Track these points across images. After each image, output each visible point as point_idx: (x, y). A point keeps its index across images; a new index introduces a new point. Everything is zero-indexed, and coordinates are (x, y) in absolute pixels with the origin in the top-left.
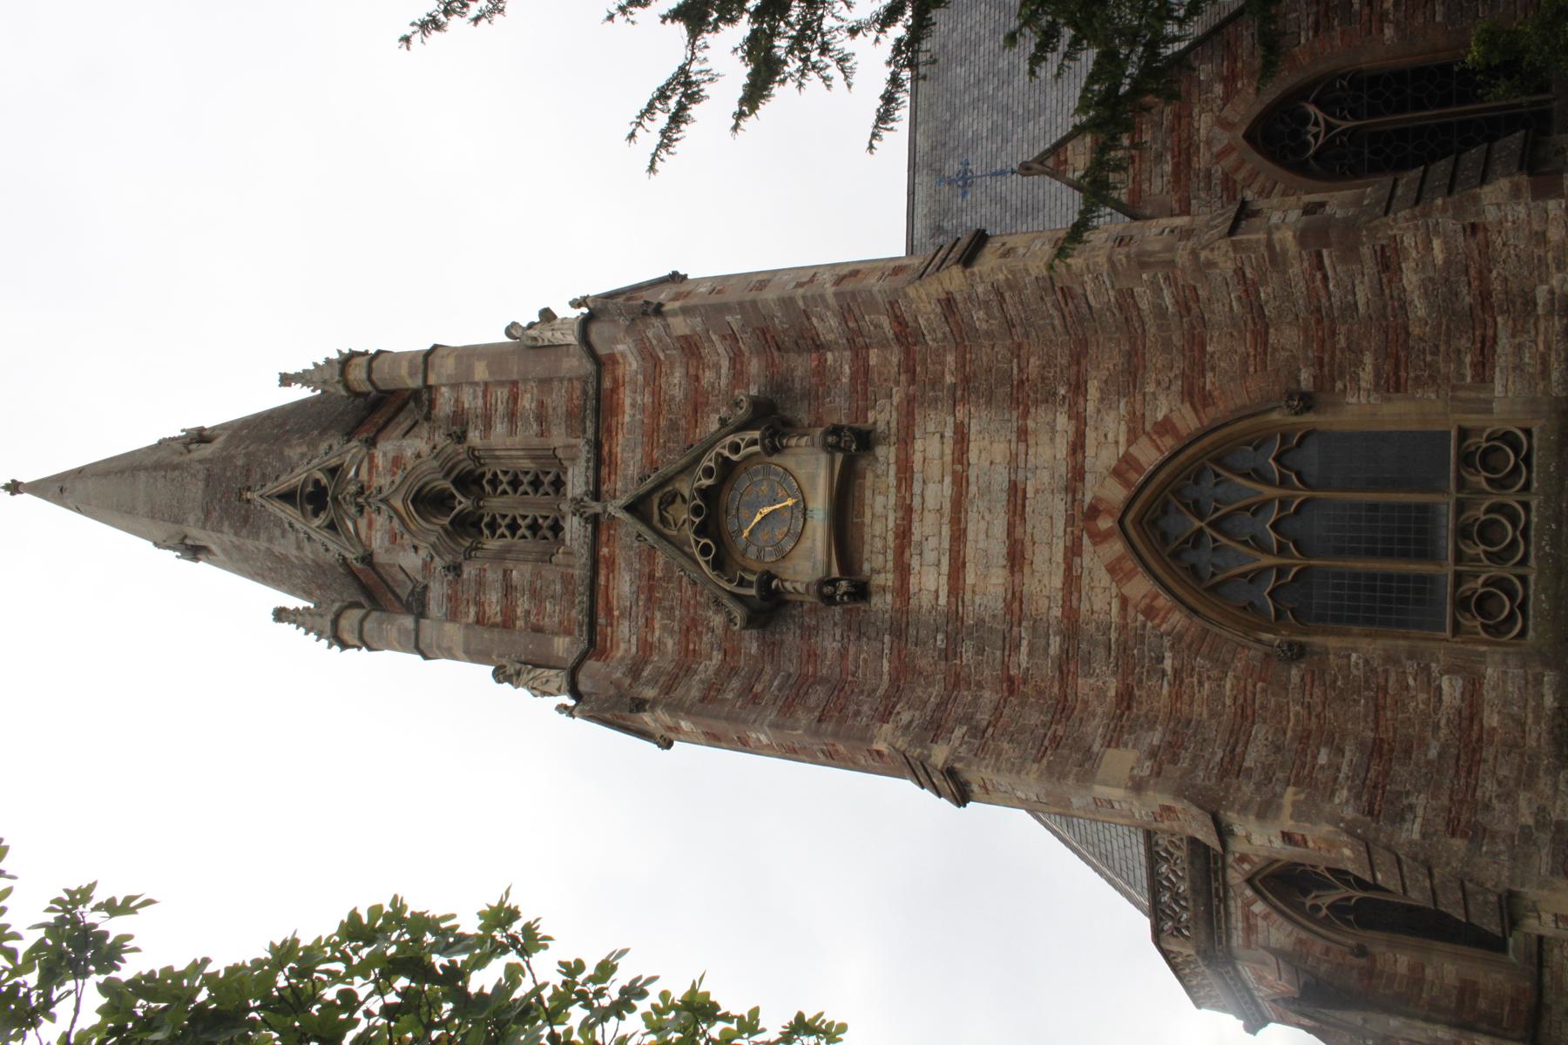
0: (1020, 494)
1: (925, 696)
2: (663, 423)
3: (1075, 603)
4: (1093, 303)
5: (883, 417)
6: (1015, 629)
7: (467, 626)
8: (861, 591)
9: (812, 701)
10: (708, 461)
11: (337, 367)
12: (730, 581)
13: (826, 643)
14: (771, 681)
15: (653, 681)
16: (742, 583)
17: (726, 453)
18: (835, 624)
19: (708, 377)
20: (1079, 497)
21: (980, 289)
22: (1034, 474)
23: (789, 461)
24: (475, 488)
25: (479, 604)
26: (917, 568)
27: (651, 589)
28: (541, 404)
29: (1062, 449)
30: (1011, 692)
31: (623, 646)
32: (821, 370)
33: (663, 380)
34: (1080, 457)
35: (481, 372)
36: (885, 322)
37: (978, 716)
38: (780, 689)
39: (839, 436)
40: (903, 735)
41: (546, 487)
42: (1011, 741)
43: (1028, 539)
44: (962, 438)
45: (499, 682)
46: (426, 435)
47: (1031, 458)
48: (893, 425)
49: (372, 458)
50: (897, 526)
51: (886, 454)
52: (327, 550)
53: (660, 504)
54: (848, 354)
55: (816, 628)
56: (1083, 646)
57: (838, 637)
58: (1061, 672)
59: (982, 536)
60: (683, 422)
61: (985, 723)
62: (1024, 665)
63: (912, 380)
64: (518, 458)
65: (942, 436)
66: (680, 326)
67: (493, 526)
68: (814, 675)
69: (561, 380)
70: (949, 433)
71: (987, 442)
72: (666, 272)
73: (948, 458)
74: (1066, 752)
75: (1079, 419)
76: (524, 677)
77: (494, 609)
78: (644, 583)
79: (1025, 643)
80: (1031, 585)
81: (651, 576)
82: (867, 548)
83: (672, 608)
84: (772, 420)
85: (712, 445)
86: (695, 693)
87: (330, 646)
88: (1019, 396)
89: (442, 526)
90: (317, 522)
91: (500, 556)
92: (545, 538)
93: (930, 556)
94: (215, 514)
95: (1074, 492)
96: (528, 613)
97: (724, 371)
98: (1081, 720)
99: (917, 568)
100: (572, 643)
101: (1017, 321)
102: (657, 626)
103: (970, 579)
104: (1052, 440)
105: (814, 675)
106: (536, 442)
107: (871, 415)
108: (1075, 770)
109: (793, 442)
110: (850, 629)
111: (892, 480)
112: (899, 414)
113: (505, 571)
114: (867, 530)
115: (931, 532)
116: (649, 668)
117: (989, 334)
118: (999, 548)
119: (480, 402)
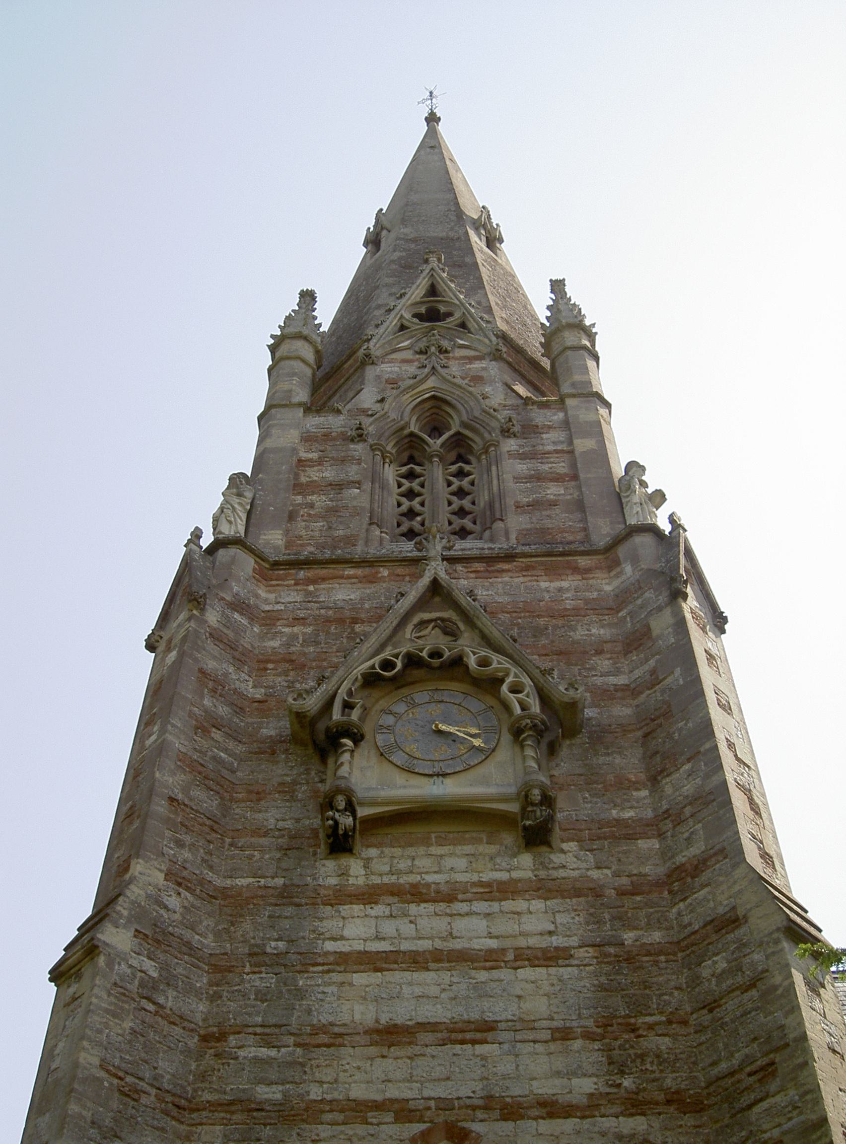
0: (478, 1036)
1: (201, 928)
2: (542, 621)
3: (328, 1117)
4: (756, 1109)
5: (569, 859)
6: (291, 1040)
7: (294, 450)
8: (340, 844)
9: (198, 793)
10: (498, 662)
11: (577, 321)
12: (350, 693)
13: (273, 811)
14: (225, 750)
15: (228, 623)
16: (348, 706)
17: (510, 680)
18: (298, 820)
19: (604, 663)
20: (480, 1114)
21: (756, 957)
22: (509, 1053)
23: (505, 752)
24: (452, 456)
25: (320, 462)
26: (373, 913)
27: (341, 621)
28: (553, 504)
29: (545, 1088)
30: (205, 1039)
31: (272, 596)
32: (623, 785)
33: (594, 618)
34: (535, 1112)
35: (582, 445)
36: (697, 849)
37: (171, 993)
38: (215, 758)
39: (541, 803)
40: (148, 896)
41: (458, 522)
42: (133, 1032)
43: (417, 1049)
44: (550, 957)
45: (232, 479)
46: (509, 402)
47: (529, 1047)
48: (562, 873)
49: (480, 358)
50: (428, 885)
51: (524, 865)
52: (377, 326)
53: (443, 620)
54: (650, 814)
55: (293, 799)
56: (268, 1131)
57: (281, 824)
58: (232, 1103)
59: (418, 991)
60: (544, 641)
61: (161, 1000)
62: (241, 1053)
63: (622, 893)
64: (490, 490)
65: (550, 933)
66: (661, 624)
67: (411, 476)
68: (232, 800)
69: (584, 520)
70: (556, 941)
71: (547, 988)
72: (723, 606)
73: (522, 942)
74: (115, 1105)
75: (589, 1108)
76: (235, 501)
77: (314, 474)
78: (348, 613)
79: (273, 1053)
80: (351, 1057)
81: (355, 621)
82: (398, 851)
83: (317, 643)
84: (555, 726)
85: (516, 663)
86: (211, 665)
87: (272, 336)
88: (614, 1030)
89: (407, 424)
90: (408, 316)
91: (375, 477)
92: (399, 525)
93: (388, 928)
94: (413, 246)
95: (486, 1108)
96: (312, 506)
97: (612, 680)
98: (163, 1130)
99: (373, 913)
100: (276, 548)
101: (718, 1013)
102: (296, 629)
103: (360, 979)
104: (558, 1074)
105: (232, 800)
106: (510, 502)
107: (572, 846)
108: (88, 1115)
109: (529, 752)
110: (292, 837)
111: (486, 877)
112: (575, 879)
113: (359, 483)
114: (422, 850)
115: (422, 927)
116: (245, 621)
117: (695, 981)
118: (402, 1013)
119: (550, 448)
